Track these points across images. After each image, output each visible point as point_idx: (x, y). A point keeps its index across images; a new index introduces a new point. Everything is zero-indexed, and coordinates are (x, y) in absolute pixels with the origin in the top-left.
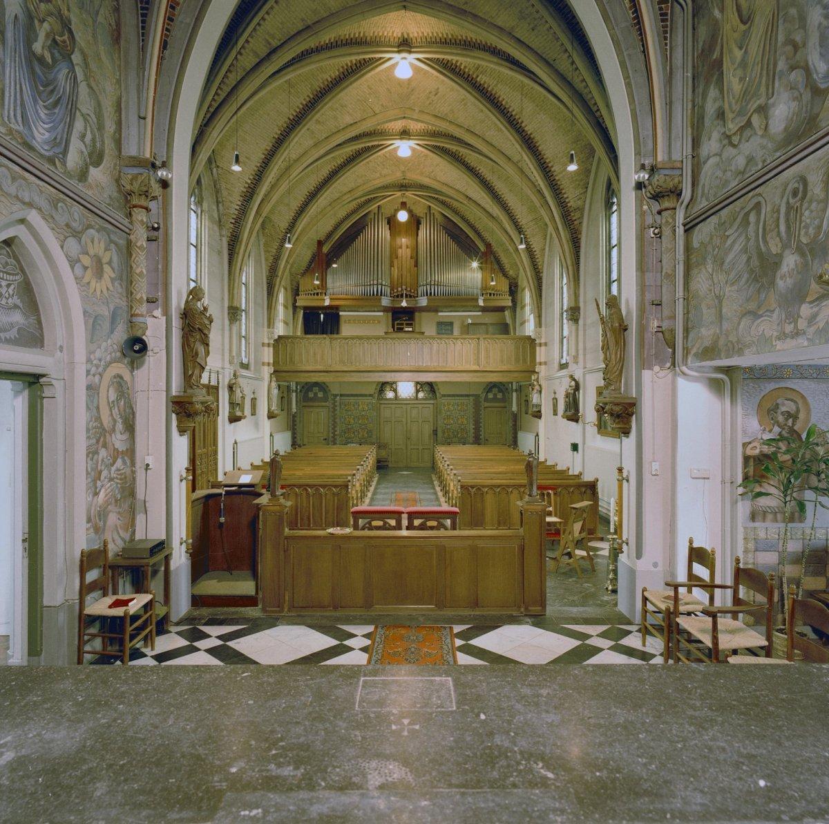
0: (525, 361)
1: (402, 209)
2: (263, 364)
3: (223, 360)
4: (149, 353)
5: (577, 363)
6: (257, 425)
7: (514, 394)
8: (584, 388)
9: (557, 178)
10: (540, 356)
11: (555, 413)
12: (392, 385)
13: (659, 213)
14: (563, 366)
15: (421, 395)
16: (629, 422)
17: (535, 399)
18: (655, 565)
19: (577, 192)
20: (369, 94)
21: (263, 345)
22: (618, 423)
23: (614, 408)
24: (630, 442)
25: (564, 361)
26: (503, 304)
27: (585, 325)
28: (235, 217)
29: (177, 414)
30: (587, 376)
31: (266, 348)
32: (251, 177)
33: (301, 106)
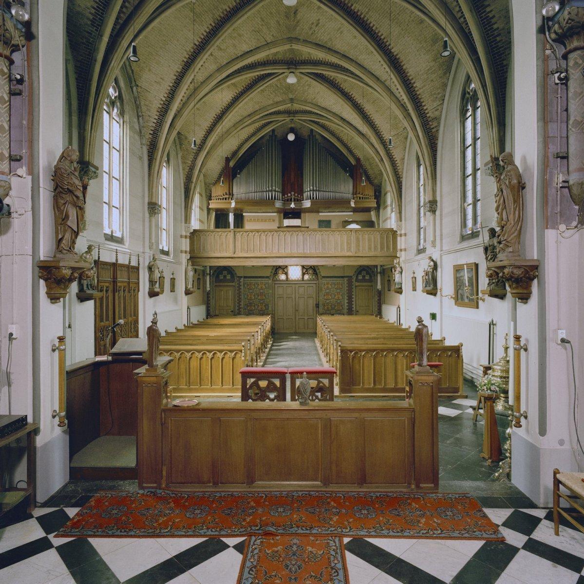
0: (388, 248)
1: (290, 132)
2: (182, 252)
3: (144, 247)
4: (14, 215)
5: (434, 246)
6: (176, 300)
7: (379, 276)
8: (441, 267)
9: (418, 93)
10: (401, 244)
11: (414, 289)
12: (284, 269)
13: (565, 57)
14: (420, 251)
15: (306, 277)
16: (528, 287)
17: (397, 278)
18: (561, 443)
19: (435, 104)
20: (262, 25)
21: (181, 237)
22: (516, 288)
23: (515, 271)
24: (528, 311)
25: (421, 247)
26: (370, 206)
27: (441, 215)
28: (153, 129)
29: (46, 280)
30: (444, 257)
31: (184, 239)
32: (166, 95)
33: (205, 34)
